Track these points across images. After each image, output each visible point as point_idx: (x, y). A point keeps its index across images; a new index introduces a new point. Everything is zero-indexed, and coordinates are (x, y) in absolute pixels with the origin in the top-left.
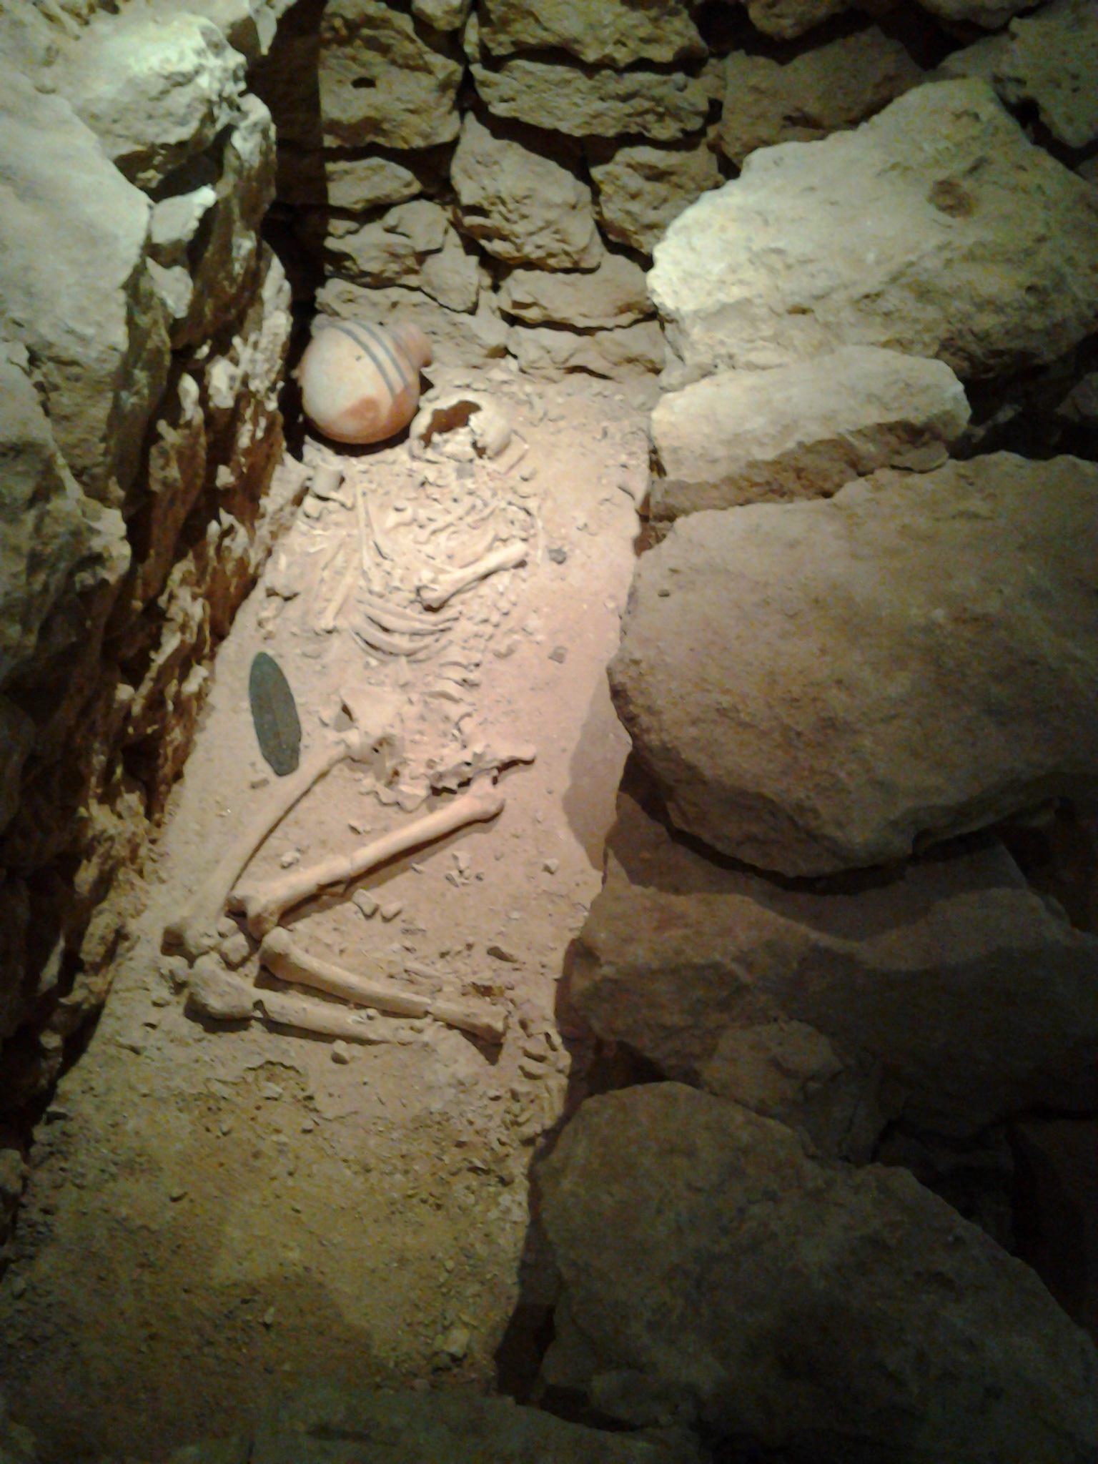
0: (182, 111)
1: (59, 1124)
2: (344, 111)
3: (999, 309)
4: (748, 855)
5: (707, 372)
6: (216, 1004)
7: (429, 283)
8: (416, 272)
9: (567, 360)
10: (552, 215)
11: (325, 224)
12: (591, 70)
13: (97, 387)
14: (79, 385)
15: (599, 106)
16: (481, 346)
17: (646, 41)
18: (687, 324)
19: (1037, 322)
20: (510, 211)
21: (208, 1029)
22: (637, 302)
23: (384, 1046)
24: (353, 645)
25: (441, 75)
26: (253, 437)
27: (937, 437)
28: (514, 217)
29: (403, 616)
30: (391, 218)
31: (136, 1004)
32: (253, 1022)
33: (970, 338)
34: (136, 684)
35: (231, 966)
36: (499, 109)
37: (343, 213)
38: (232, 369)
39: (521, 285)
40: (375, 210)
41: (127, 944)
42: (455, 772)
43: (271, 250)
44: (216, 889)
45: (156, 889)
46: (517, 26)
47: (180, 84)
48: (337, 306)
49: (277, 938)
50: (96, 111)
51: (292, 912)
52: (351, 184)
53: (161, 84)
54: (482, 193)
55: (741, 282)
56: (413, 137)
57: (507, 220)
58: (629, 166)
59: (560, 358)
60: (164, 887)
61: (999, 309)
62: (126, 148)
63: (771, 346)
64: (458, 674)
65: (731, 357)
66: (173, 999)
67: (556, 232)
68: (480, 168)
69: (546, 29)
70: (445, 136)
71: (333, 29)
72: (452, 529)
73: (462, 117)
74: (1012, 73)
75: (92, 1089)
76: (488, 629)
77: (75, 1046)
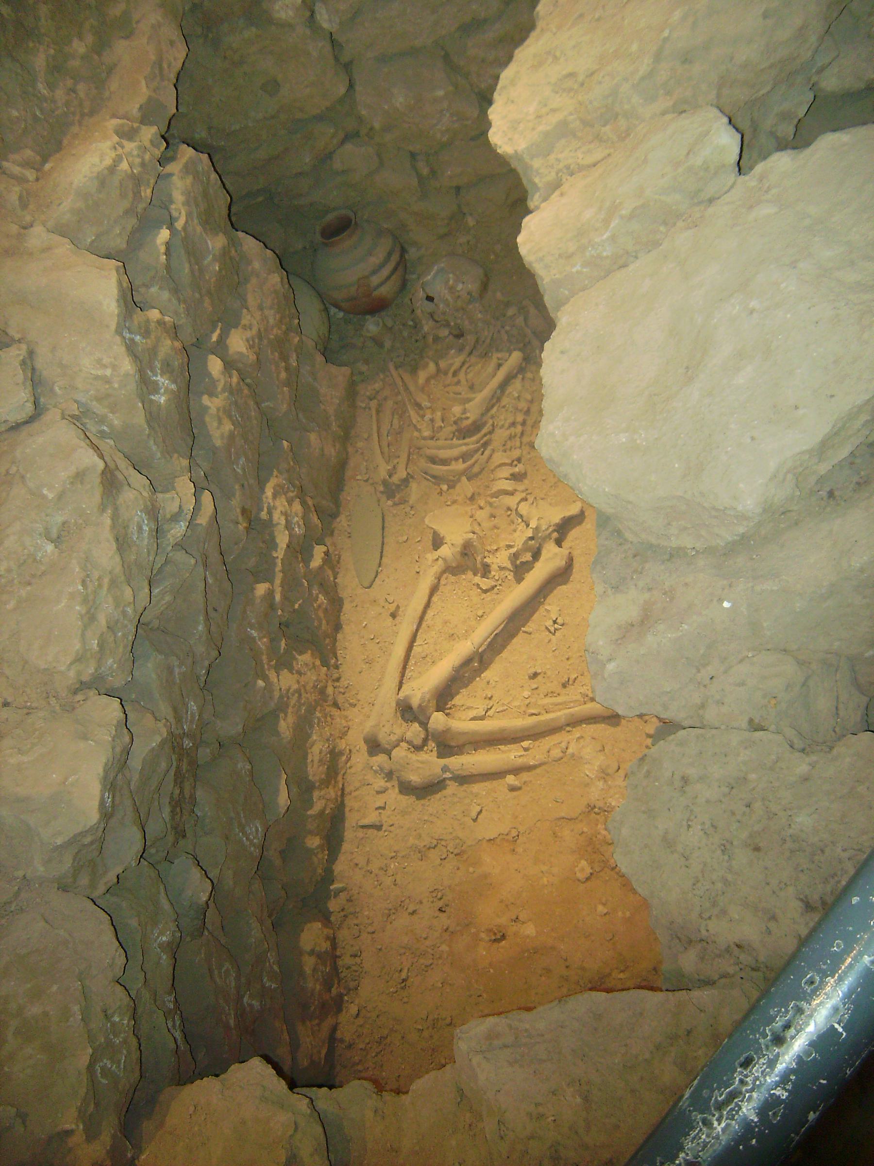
1: (342, 895)
6: (415, 778)
21: (419, 798)
23: (544, 767)
24: (426, 483)
29: (451, 447)
31: (371, 798)
32: (448, 782)
34: (270, 579)
35: (418, 748)
41: (344, 758)
42: (526, 548)
44: (387, 696)
45: (351, 713)
49: (438, 720)
51: (444, 697)
55: (553, 111)
60: (355, 710)
64: (506, 472)
65: (568, 167)
66: (389, 785)
72: (466, 366)
75: (357, 865)
77: (333, 839)
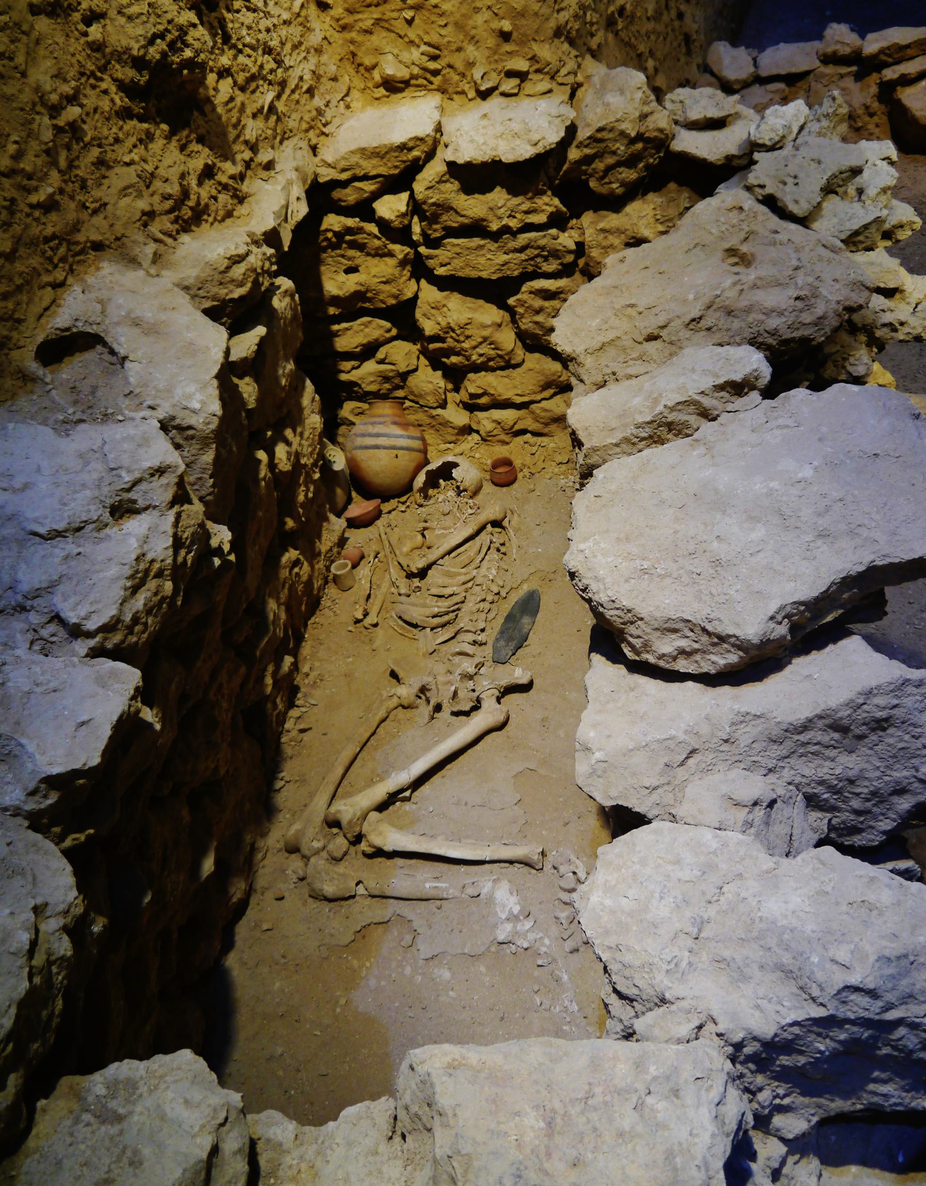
0: (241, 278)
2: (341, 288)
3: (781, 314)
4: (682, 666)
5: (602, 385)
6: (329, 889)
7: (412, 393)
8: (402, 388)
9: (512, 427)
10: (486, 333)
11: (335, 365)
12: (496, 236)
13: (204, 442)
14: (194, 442)
15: (506, 257)
17: (527, 212)
18: (581, 359)
19: (807, 318)
25: (401, 256)
27: (753, 388)
28: (462, 339)
30: (380, 355)
33: (766, 335)
36: (440, 271)
37: (348, 356)
38: (287, 448)
39: (475, 383)
40: (368, 351)
46: (444, 218)
47: (239, 262)
48: (352, 418)
50: (186, 283)
52: (351, 336)
53: (226, 263)
56: (387, 297)
57: (458, 341)
58: (531, 293)
61: (781, 314)
62: (208, 304)
63: (640, 362)
64: (470, 637)
65: (614, 374)
68: (433, 311)
69: (463, 216)
70: (409, 294)
71: (327, 239)
73: (418, 283)
74: (756, 183)
76: (486, 606)
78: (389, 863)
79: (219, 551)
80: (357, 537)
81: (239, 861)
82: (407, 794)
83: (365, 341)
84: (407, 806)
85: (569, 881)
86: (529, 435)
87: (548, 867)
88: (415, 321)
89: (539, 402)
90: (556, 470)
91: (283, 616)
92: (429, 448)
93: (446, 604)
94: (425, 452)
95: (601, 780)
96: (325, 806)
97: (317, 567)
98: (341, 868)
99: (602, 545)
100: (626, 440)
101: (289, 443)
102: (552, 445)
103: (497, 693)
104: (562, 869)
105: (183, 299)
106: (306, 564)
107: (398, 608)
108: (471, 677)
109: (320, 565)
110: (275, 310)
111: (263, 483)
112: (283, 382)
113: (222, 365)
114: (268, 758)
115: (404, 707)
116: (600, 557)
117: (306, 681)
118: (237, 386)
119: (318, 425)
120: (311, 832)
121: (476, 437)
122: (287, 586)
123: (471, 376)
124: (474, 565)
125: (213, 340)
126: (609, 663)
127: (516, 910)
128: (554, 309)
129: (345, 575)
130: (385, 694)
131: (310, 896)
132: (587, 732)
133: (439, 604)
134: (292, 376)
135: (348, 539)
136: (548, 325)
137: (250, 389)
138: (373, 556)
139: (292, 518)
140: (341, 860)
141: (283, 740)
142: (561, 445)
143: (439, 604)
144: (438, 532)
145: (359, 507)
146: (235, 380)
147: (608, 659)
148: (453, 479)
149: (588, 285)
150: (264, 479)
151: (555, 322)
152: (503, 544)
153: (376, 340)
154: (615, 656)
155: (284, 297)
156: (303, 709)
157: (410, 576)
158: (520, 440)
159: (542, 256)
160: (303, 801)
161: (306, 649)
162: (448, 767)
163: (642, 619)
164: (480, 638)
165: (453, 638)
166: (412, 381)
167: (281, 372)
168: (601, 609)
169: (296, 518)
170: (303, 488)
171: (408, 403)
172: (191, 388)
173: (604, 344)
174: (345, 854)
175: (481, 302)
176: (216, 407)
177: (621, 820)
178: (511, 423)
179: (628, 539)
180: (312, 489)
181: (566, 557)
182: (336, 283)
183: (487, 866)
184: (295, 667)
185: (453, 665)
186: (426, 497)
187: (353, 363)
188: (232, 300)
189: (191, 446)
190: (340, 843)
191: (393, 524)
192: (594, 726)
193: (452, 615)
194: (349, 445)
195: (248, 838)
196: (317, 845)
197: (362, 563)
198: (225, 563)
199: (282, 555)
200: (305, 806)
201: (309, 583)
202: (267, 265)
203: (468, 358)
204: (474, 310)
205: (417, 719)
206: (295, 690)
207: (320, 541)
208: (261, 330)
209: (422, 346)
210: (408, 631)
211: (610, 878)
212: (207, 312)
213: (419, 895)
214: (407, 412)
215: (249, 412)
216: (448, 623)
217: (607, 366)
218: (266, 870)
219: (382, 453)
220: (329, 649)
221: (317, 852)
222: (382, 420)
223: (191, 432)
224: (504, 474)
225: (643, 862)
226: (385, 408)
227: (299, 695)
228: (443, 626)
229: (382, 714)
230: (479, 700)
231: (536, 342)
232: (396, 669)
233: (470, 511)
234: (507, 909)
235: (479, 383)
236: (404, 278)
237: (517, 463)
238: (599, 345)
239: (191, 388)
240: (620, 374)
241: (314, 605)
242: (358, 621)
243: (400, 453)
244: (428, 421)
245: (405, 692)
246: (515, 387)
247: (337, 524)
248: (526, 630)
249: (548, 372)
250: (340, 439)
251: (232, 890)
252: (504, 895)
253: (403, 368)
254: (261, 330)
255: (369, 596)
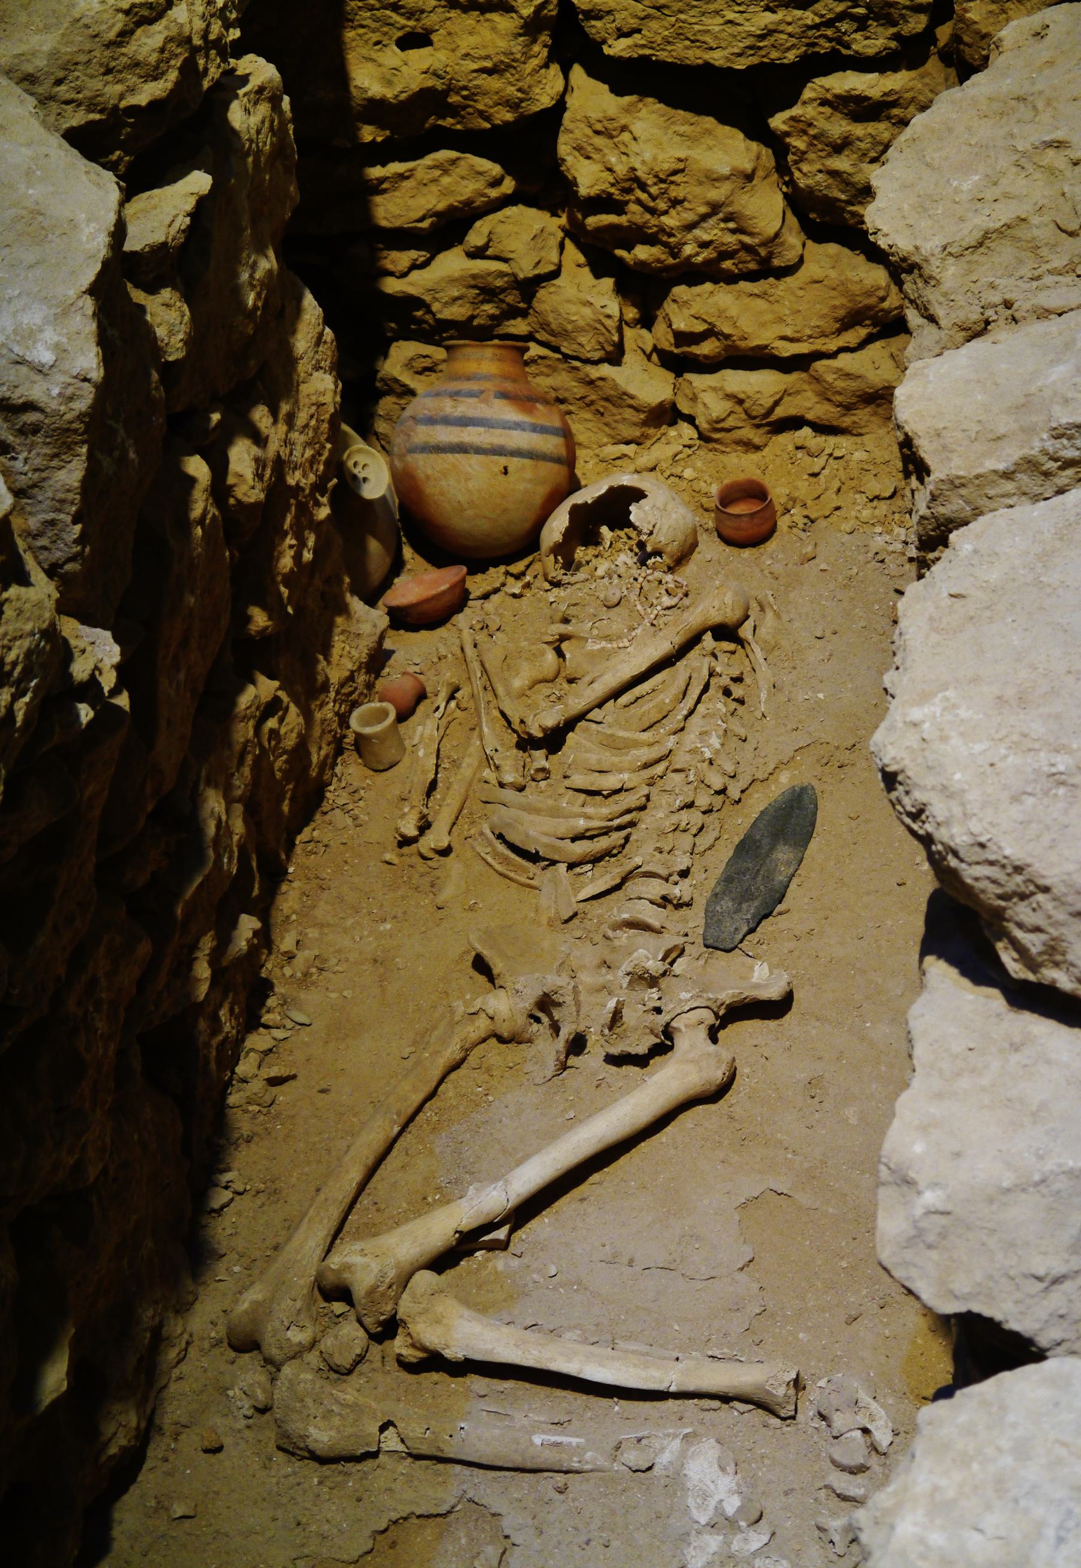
0: (153, 58)
2: (389, 83)
5: (977, 331)
6: (321, 1436)
7: (545, 326)
8: (524, 314)
10: (716, 194)
11: (374, 257)
14: (39, 439)
16: (637, 409)
18: (933, 268)
20: (654, 198)
22: (869, 308)
26: (298, 557)
28: (662, 205)
30: (476, 237)
36: (618, 48)
37: (402, 238)
38: (255, 451)
39: (689, 308)
40: (448, 229)
43: (302, 284)
47: (151, 21)
48: (407, 379)
50: (29, 68)
52: (409, 194)
54: (606, 175)
56: (494, 103)
57: (652, 211)
58: (824, 102)
59: (758, 411)
62: (77, 118)
63: (1069, 279)
64: (656, 888)
65: (1008, 305)
67: (726, 220)
68: (599, 141)
70: (545, 101)
73: (566, 72)
76: (694, 818)
78: (455, 1384)
79: (90, 689)
80: (411, 651)
81: (127, 1366)
82: (501, 1234)
83: (441, 206)
84: (500, 1261)
85: (854, 1450)
86: (806, 431)
87: (807, 1413)
88: (556, 163)
89: (833, 355)
90: (866, 513)
91: (238, 827)
92: (580, 453)
93: (605, 811)
94: (569, 462)
95: (934, 1255)
96: (319, 1252)
97: (318, 716)
98: (349, 1392)
99: (963, 713)
100: (1030, 465)
101: (260, 440)
102: (859, 455)
103: (709, 1018)
104: (839, 1421)
105: (20, 107)
106: (293, 709)
107: (500, 815)
108: (653, 982)
109: (327, 712)
110: (235, 133)
111: (199, 531)
112: (251, 299)
113: (105, 264)
114: (201, 1141)
115: (501, 1040)
116: (955, 741)
117: (288, 971)
118: (142, 309)
119: (328, 398)
120: (285, 1308)
121: (686, 431)
122: (249, 759)
123: (680, 291)
124: (671, 724)
125: (86, 204)
126: (966, 982)
127: (732, 1504)
128: (876, 142)
129: (381, 737)
130: (460, 1009)
131: (279, 1448)
132: (906, 1141)
133: (589, 810)
134: (270, 283)
135: (390, 654)
136: (858, 178)
137: (173, 316)
138: (448, 694)
139: (264, 607)
140: (350, 1372)
141: (232, 1100)
142: (881, 455)
143: (589, 810)
144: (593, 646)
145: (419, 582)
146: (138, 296)
147: (964, 973)
148: (631, 525)
149: (956, 92)
150: (201, 521)
151: (876, 176)
152: (738, 680)
153: (468, 203)
154: (982, 968)
155: (255, 100)
156: (279, 1034)
157: (526, 743)
158: (786, 440)
159: (854, 18)
160: (271, 1238)
161: (289, 899)
162: (595, 1177)
163: (1046, 890)
164: (676, 891)
165: (617, 888)
166: (546, 299)
167: (245, 276)
168: (953, 862)
169: (274, 609)
170: (290, 541)
171: (535, 350)
172: (34, 317)
173: (986, 235)
174: (360, 1359)
175: (709, 122)
176: (89, 360)
177: (983, 1348)
178: (768, 402)
179: (1022, 701)
180: (311, 541)
181: (879, 736)
182: (379, 72)
183: (670, 1403)
184: (264, 939)
185: (613, 949)
186: (570, 565)
187: (413, 254)
188: (133, 110)
189: (31, 447)
190: (350, 1336)
191: (494, 622)
192: (924, 1129)
193: (617, 837)
194: (399, 442)
195: (147, 1315)
196: (297, 1336)
197: (421, 709)
198: (105, 710)
199: (241, 690)
200: (276, 1248)
201: (301, 751)
202: (216, 27)
203: (674, 251)
204: (691, 140)
205: (528, 1067)
206: (261, 990)
207: (327, 658)
208: (199, 182)
209: (571, 219)
210: (518, 869)
211: (944, 1482)
212: (76, 138)
213: (518, 1460)
214: (532, 369)
215: (169, 370)
216: (608, 853)
217: (993, 286)
218: (185, 1386)
219: (473, 464)
220: (341, 899)
221: (298, 1353)
222: (474, 386)
223: (32, 417)
224: (746, 519)
225: (1022, 1451)
226: (483, 361)
227: (271, 1002)
228: (596, 860)
229: (452, 1052)
230: (668, 1032)
231: (832, 218)
232: (486, 953)
233: (667, 601)
234: (712, 1503)
235: (696, 308)
236: (534, 62)
237: (778, 493)
238: (977, 235)
239: (34, 317)
240: (1022, 306)
241: (311, 799)
242: (406, 841)
243: (514, 463)
244: (580, 391)
245: (505, 1006)
246: (780, 320)
247: (367, 620)
248: (781, 878)
249: (856, 288)
250: (381, 427)
251: (109, 1429)
252: (707, 1472)
253: (525, 269)
254: (199, 182)
255: (433, 786)
